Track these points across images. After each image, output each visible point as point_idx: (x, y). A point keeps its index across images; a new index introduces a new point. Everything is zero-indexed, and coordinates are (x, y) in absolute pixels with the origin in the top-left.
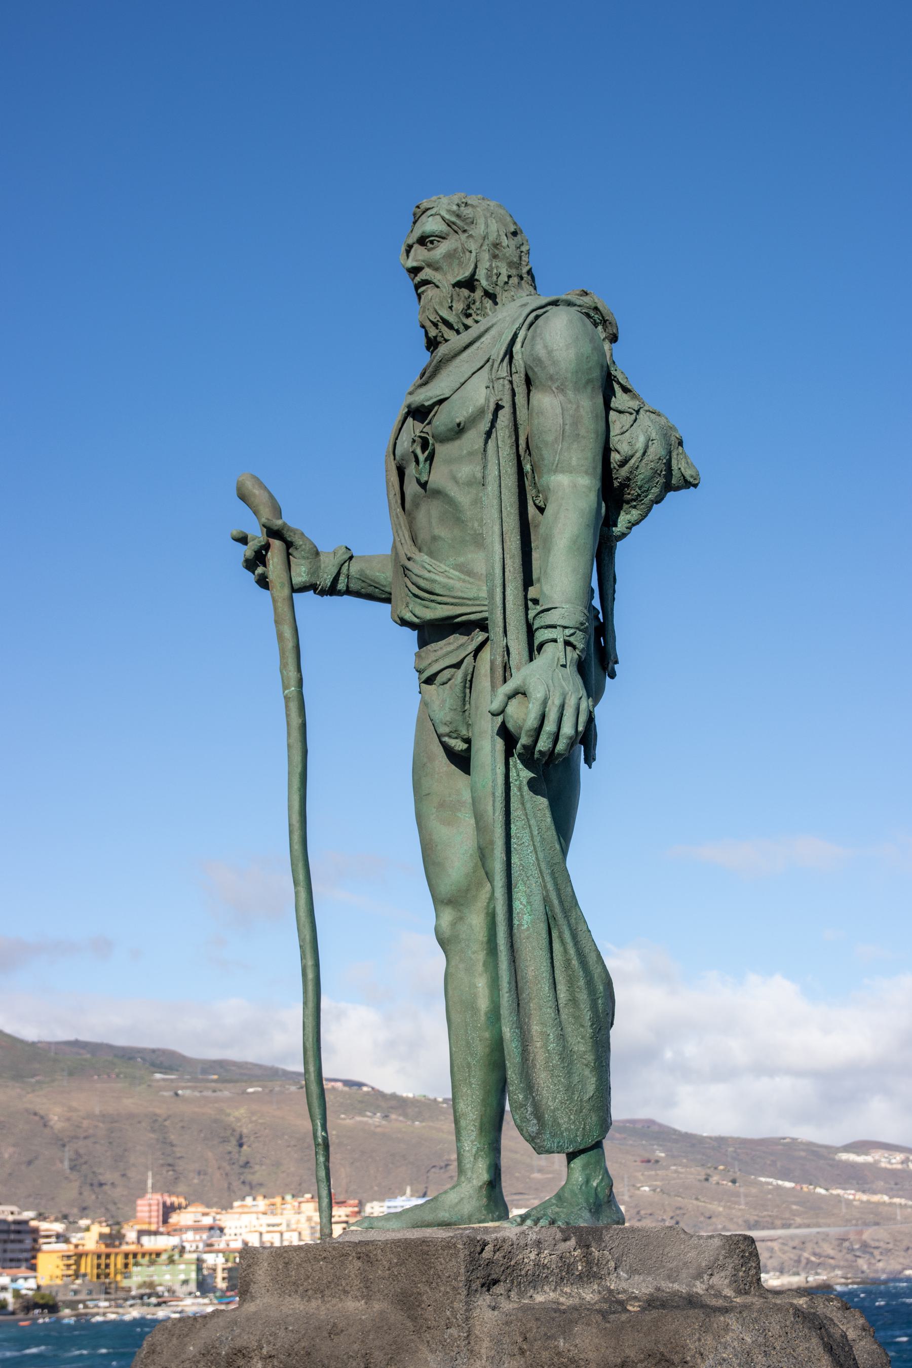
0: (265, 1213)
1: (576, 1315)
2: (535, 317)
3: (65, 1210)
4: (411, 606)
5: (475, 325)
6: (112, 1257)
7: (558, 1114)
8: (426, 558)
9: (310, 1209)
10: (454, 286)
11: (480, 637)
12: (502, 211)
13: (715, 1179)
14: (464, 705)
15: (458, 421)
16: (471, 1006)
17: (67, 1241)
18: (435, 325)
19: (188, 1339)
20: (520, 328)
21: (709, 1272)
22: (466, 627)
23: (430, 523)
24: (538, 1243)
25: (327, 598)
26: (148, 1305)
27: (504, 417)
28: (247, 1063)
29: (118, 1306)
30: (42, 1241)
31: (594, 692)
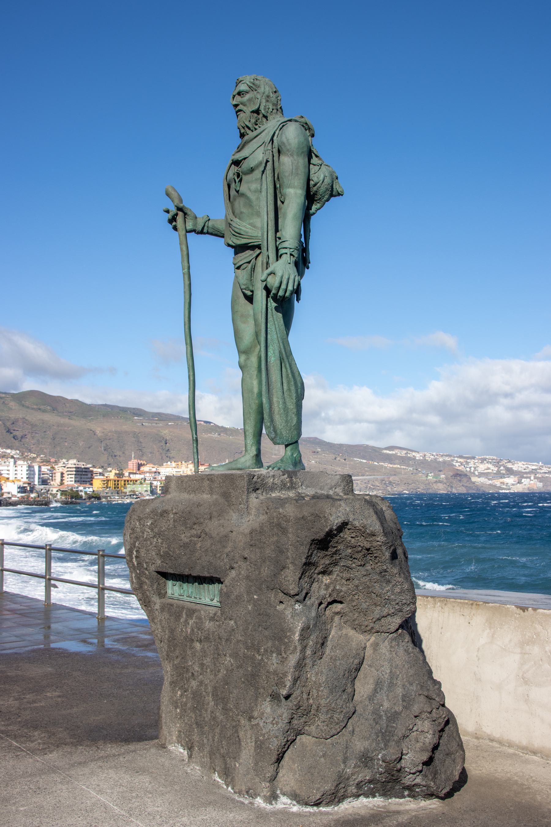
0: (175, 468)
1: (286, 501)
2: (283, 126)
3: (102, 465)
4: (232, 239)
5: (259, 128)
6: (120, 481)
7: (282, 431)
8: (238, 220)
9: (191, 467)
10: (251, 112)
11: (258, 251)
12: (271, 83)
13: (338, 459)
14: (251, 277)
15: (251, 166)
16: (251, 391)
17: (103, 475)
18: (244, 128)
19: (146, 507)
20: (276, 130)
21: (335, 487)
22: (253, 248)
23: (240, 206)
24: (274, 476)
25: (200, 235)
26: (133, 498)
27: (270, 165)
28: (168, 414)
29: (122, 498)
30: (94, 475)
31: (301, 274)
